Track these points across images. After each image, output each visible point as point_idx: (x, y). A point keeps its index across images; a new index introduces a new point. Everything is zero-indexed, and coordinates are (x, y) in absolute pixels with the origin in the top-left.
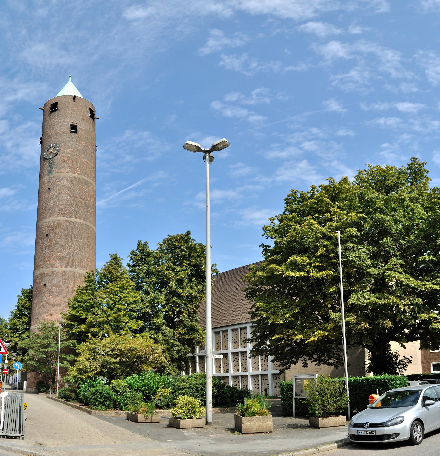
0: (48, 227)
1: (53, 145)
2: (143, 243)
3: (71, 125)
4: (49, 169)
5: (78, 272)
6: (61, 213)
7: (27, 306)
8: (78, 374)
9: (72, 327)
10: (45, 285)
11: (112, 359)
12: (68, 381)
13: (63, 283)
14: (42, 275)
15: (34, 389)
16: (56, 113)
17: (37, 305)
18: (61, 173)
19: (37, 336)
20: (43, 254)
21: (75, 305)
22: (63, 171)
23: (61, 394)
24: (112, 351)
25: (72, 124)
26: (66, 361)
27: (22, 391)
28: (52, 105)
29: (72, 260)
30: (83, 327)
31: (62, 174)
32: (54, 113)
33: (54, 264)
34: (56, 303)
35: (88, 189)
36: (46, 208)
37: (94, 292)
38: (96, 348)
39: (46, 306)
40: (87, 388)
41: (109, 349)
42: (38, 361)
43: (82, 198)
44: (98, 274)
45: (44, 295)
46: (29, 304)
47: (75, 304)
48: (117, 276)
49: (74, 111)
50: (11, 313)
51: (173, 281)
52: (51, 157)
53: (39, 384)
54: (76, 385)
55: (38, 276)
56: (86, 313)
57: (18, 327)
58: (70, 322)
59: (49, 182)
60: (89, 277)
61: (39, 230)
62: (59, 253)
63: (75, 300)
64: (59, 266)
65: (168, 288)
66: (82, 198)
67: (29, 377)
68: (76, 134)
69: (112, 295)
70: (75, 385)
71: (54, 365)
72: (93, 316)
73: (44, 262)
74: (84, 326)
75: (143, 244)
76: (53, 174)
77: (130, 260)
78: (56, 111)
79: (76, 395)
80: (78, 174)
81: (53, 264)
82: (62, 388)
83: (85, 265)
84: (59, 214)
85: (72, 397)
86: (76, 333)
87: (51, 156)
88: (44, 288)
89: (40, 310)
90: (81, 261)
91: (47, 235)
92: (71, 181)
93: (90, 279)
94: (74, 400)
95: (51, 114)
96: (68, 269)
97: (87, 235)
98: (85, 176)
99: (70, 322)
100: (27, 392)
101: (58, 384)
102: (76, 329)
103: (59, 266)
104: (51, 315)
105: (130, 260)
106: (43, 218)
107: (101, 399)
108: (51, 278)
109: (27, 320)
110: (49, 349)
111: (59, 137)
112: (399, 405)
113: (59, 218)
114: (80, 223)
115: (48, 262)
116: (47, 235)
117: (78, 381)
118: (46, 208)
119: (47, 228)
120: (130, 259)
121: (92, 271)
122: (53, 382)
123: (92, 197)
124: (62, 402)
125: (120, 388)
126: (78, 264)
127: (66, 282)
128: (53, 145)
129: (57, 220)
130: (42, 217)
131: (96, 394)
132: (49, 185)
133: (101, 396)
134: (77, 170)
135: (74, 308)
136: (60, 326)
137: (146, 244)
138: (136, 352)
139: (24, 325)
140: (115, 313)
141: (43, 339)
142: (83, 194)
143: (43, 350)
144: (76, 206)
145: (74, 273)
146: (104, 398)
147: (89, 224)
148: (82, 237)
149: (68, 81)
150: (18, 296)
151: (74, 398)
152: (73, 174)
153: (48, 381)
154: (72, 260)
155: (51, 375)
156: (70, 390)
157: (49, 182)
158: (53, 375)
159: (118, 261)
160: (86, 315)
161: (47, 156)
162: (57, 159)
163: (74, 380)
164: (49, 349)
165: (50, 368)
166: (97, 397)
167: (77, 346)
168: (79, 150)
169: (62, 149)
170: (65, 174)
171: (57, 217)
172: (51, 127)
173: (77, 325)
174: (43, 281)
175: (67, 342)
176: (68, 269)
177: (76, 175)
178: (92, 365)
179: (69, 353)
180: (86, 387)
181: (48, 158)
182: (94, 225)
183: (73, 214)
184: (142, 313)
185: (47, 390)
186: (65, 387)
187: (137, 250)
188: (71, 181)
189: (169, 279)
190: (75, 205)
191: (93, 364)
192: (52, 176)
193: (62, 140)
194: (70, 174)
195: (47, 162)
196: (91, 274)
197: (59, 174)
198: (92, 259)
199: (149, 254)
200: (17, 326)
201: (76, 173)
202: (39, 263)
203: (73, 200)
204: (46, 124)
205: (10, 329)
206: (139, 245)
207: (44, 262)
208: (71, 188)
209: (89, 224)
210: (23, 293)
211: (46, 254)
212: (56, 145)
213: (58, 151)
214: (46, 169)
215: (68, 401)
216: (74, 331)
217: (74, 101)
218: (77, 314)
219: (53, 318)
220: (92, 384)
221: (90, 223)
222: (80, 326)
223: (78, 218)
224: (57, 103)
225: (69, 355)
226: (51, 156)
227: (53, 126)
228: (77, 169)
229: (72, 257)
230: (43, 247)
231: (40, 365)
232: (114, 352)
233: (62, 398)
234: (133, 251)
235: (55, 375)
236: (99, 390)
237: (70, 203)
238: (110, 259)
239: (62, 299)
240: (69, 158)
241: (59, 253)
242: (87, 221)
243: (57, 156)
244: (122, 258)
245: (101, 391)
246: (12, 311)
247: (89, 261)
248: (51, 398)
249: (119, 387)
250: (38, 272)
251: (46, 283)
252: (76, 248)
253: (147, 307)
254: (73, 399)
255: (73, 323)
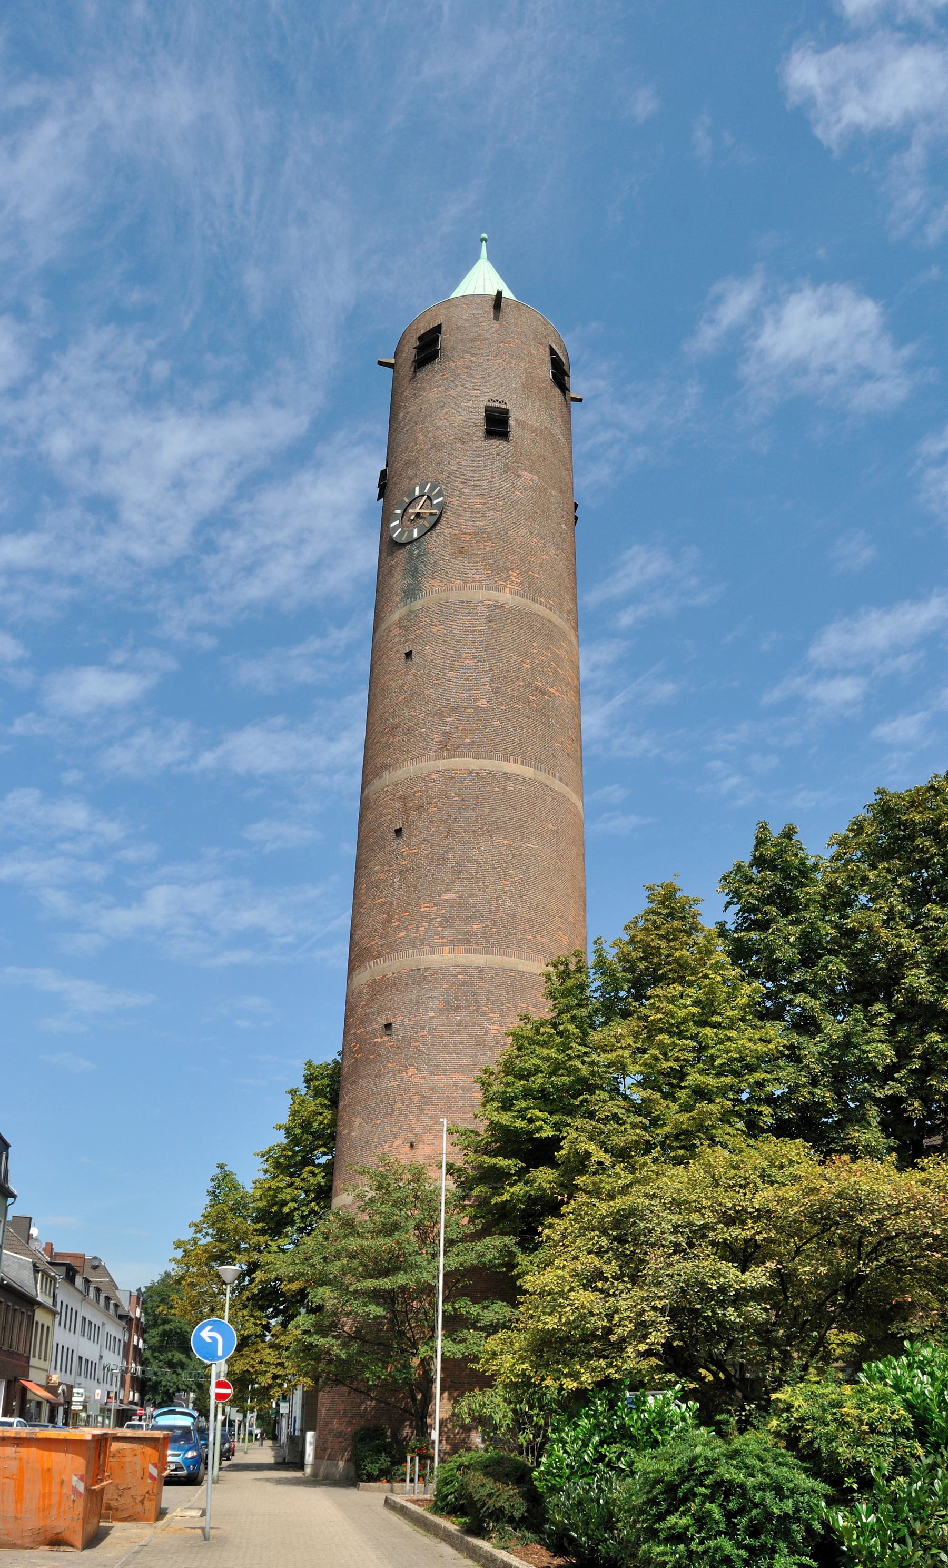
0: (403, 799)
1: (422, 488)
2: (775, 831)
3: (488, 409)
4: (409, 580)
5: (521, 968)
6: (452, 742)
7: (322, 1122)
8: (535, 1366)
9: (495, 1177)
10: (388, 1026)
11: (730, 1271)
12: (482, 1421)
13: (458, 1014)
14: (379, 986)
15: (341, 1464)
16: (436, 365)
17: (358, 1108)
18: (452, 590)
19: (349, 1225)
20: (383, 904)
21: (509, 1090)
22: (458, 583)
23: (445, 1490)
24: (730, 1221)
25: (491, 404)
26: (476, 1328)
27: (298, 1474)
28: (420, 338)
29: (495, 924)
30: (545, 1177)
31: (454, 596)
32: (429, 367)
33: (423, 942)
34: (432, 1097)
35: (553, 652)
36: (394, 728)
37: (588, 1034)
38: (633, 1212)
39: (392, 1110)
40: (590, 1449)
41: (708, 1213)
42: (358, 1336)
43: (529, 685)
44: (601, 965)
45: (385, 1067)
46: (328, 1114)
47: (508, 1085)
48: (682, 965)
49: (498, 354)
50: (263, 1156)
51: (917, 965)
52: (415, 535)
53: (361, 1440)
54: (522, 1439)
55: (360, 992)
56: (556, 1118)
57: (286, 1210)
58: (489, 1160)
59: (406, 628)
60: (564, 975)
61: (370, 816)
62: (444, 897)
63: (508, 1068)
64: (443, 945)
65: (899, 998)
66: (529, 685)
67: (323, 1410)
68: (505, 444)
69: (665, 1038)
70: (515, 1436)
71: (423, 1350)
72: (589, 1124)
73: (384, 936)
74: (550, 1171)
75: (777, 835)
76: (424, 596)
77: (730, 903)
78: (437, 360)
79: (523, 1496)
80: (513, 593)
81: (421, 940)
82: (455, 1450)
83: (546, 940)
84: (443, 746)
85: (501, 1509)
86: (515, 1206)
87: (416, 531)
88: (386, 1038)
89: (368, 1127)
90: (532, 927)
91: (398, 832)
92: (490, 620)
93: (570, 983)
94: (517, 1523)
95: (420, 375)
96: (478, 959)
97: (550, 826)
98: (541, 603)
99: (489, 1160)
100: (315, 1481)
101: (435, 1435)
102: (516, 1189)
103: (443, 945)
104: (412, 1146)
105: (730, 903)
106: (385, 767)
107: (731, 1533)
108: (413, 996)
109: (320, 1179)
110: (400, 1279)
111: (446, 455)
112: (179, 1432)
113: (443, 764)
114: (524, 780)
115: (402, 934)
116: (398, 832)
117: (530, 1417)
118: (394, 728)
119: (398, 805)
120: (728, 899)
121: (577, 954)
122: (423, 1430)
123: (567, 684)
124: (446, 1537)
125: (858, 1441)
126: (519, 936)
127: (472, 1009)
128: (422, 488)
129: (438, 772)
130: (378, 765)
131: (689, 1496)
132: (406, 641)
133: (729, 1516)
134: (508, 577)
135: (506, 1104)
136: (446, 1185)
137: (788, 834)
138: (877, 1216)
139: (310, 1202)
140: (686, 1108)
141: (376, 1233)
142: (533, 668)
143: (370, 1283)
144: (508, 715)
145: (503, 972)
146: (754, 1530)
147: (557, 785)
148: (531, 833)
149: (477, 258)
150: (293, 1092)
151: (517, 1515)
152: (494, 595)
153: (401, 1423)
154: (495, 924)
155: (414, 1399)
156: (494, 1469)
157: (406, 628)
158: (419, 1397)
159: (684, 908)
160: (557, 1126)
161: (401, 534)
162: (437, 539)
163: (510, 1414)
164: (400, 1279)
165: (407, 1366)
166: (701, 1521)
167: (521, 1258)
168: (516, 502)
169: (454, 501)
170: (466, 595)
171: (437, 758)
172: (416, 423)
173: (521, 1173)
174: (381, 1011)
175: (479, 1246)
176: (478, 959)
177: (506, 597)
178: (617, 1311)
179: (487, 1298)
180: (585, 1445)
181: (403, 540)
182: (577, 793)
183: (497, 744)
184: (795, 1108)
185: (394, 1464)
186: (469, 1449)
187: (751, 866)
188: (490, 620)
189: (900, 960)
190: (506, 712)
191: (623, 1305)
192: (417, 604)
193: (455, 468)
194: (483, 595)
195: (402, 554)
196: (572, 967)
197: (443, 595)
198: (571, 919)
199: (805, 873)
200: (284, 1203)
201: (507, 590)
202: (365, 943)
203: (495, 693)
204: (402, 415)
205: (257, 1220)
206: (760, 842)
207: (384, 936)
208: (486, 648)
209: (557, 785)
210: (308, 1080)
211: (391, 904)
212: (432, 488)
213: (442, 508)
214: (399, 581)
215: (478, 1530)
216: (506, 1197)
217: (496, 318)
218: (520, 1124)
219: (423, 1152)
220: (622, 1426)
221: (560, 780)
222: (534, 1173)
223: (516, 762)
224: (438, 329)
225: (485, 1303)
226: (416, 531)
227: (426, 417)
228: (509, 576)
229: (496, 911)
230: (382, 876)
231: (360, 1353)
232: (736, 1233)
233: (452, 1510)
234: (739, 868)
235: (428, 1398)
236: (712, 1463)
237: (483, 703)
238: (647, 906)
239: (456, 1076)
240: (479, 534)
241: (444, 897)
242: (549, 773)
243: (438, 528)
244: (696, 896)
245: (729, 1473)
246: (265, 1149)
247: (559, 928)
248: (402, 1511)
249: (845, 1437)
250: (364, 977)
251: (392, 1020)
252: (511, 876)
253: (814, 1082)
254: (511, 1520)
255: (501, 1162)
